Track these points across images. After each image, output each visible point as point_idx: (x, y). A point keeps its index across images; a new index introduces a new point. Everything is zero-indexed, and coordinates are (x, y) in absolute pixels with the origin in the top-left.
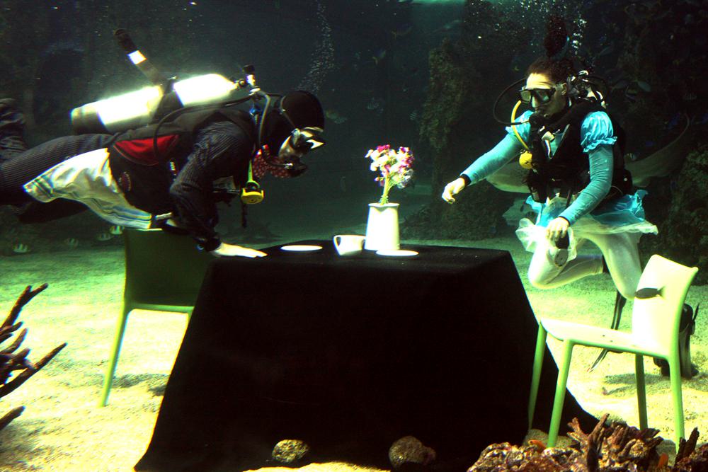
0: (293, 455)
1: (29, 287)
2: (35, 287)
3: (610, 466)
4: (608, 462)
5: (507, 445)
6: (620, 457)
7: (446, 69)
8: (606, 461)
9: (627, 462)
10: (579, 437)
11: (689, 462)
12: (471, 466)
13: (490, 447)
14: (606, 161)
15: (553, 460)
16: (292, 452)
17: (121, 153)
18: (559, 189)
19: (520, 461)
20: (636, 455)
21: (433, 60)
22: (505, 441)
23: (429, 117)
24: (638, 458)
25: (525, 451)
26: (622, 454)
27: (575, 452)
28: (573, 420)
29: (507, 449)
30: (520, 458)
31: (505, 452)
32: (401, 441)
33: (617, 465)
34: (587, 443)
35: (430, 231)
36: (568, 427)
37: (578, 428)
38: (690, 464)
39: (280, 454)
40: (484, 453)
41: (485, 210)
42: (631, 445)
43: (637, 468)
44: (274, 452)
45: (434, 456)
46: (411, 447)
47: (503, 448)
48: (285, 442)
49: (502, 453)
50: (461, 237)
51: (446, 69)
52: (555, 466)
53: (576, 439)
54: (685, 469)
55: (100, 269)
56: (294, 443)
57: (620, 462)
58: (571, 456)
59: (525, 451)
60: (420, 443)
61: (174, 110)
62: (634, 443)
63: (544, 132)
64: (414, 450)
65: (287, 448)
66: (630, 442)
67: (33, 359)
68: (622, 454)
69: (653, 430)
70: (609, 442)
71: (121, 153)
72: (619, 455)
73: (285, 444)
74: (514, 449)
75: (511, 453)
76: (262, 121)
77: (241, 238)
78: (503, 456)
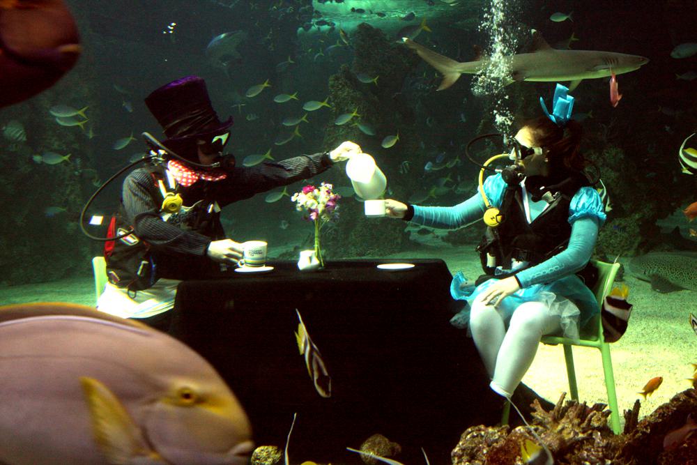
0: (270, 460)
4: (572, 433)
5: (482, 427)
6: (583, 428)
8: (570, 433)
10: (542, 415)
11: (647, 423)
12: (454, 447)
13: (470, 430)
14: (593, 235)
15: (528, 435)
16: (269, 457)
17: (501, 251)
18: (177, 282)
19: (497, 440)
20: (596, 425)
21: (333, 86)
22: (480, 424)
23: (332, 141)
24: (598, 427)
25: (498, 431)
28: (535, 402)
29: (483, 431)
30: (497, 437)
31: (483, 433)
32: (370, 439)
33: (581, 435)
34: (550, 419)
35: (338, 250)
37: (541, 408)
38: (649, 425)
39: (259, 459)
40: (463, 435)
41: (390, 226)
42: (592, 417)
44: (253, 458)
45: (400, 450)
46: (380, 443)
47: (480, 430)
48: (262, 448)
50: (369, 254)
51: (345, 94)
53: (540, 418)
54: (645, 430)
56: (270, 448)
57: (583, 433)
59: (498, 431)
60: (387, 439)
61: (470, 222)
62: (595, 414)
63: (545, 191)
64: (383, 446)
65: (265, 454)
66: (591, 414)
68: (584, 425)
69: (602, 405)
70: (571, 417)
71: (501, 251)
72: (581, 426)
73: (262, 450)
74: (490, 430)
75: (488, 433)
76: (180, 157)
78: (482, 436)
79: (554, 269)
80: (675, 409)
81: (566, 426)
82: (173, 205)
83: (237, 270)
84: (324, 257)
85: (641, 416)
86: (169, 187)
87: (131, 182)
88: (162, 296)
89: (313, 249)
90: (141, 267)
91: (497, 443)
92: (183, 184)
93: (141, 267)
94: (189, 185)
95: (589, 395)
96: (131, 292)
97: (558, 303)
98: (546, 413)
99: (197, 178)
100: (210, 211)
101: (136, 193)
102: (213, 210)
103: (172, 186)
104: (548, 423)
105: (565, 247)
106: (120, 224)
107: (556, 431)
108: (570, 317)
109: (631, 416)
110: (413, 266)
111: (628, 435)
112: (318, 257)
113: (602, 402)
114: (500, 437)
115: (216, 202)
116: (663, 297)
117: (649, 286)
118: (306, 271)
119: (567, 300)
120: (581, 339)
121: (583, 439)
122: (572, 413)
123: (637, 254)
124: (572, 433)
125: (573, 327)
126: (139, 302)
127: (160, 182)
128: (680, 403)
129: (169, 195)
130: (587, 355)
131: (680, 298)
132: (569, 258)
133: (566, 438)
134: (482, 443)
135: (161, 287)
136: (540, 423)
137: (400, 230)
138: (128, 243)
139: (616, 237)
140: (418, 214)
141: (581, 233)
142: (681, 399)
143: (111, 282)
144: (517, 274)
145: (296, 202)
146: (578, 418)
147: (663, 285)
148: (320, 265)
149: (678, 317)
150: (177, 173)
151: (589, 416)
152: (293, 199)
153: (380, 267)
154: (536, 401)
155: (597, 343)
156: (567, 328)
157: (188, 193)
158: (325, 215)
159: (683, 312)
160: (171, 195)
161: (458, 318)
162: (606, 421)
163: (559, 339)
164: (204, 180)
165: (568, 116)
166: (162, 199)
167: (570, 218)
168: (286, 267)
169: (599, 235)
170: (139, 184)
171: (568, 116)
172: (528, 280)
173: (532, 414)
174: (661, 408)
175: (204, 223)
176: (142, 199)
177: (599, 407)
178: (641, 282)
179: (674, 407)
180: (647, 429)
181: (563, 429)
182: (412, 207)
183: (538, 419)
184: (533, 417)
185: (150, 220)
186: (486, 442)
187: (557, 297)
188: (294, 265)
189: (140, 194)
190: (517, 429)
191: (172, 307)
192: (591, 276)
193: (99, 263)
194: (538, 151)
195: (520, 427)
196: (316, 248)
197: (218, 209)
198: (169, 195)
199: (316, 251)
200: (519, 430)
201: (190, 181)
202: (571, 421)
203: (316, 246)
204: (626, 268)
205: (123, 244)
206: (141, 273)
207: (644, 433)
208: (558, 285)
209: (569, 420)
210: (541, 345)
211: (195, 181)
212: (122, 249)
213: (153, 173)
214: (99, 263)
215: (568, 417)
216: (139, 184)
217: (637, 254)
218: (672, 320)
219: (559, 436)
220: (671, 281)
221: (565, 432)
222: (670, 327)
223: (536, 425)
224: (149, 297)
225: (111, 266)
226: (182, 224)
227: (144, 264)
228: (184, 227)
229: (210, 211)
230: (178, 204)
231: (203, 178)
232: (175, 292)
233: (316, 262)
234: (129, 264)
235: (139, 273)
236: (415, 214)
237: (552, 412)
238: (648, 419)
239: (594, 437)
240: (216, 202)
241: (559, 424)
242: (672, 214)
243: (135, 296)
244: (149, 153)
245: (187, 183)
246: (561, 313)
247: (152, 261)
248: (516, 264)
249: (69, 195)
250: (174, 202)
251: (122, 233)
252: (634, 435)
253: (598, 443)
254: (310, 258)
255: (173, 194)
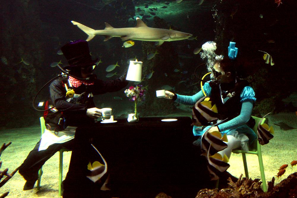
1: (5, 144)
2: (7, 144)
3: (246, 193)
4: (245, 192)
5: (206, 189)
6: (250, 190)
7: (149, 46)
8: (244, 192)
9: (253, 191)
13: (201, 191)
14: (251, 108)
15: (226, 193)
18: (76, 128)
25: (213, 191)
26: (250, 188)
27: (232, 190)
29: (207, 191)
30: (213, 194)
31: (207, 192)
32: (159, 195)
33: (249, 193)
34: (236, 186)
36: (227, 181)
38: (278, 188)
42: (254, 185)
43: (257, 192)
47: (206, 191)
49: (206, 192)
51: (149, 46)
52: (227, 195)
53: (231, 185)
55: (12, 138)
57: (250, 191)
58: (230, 191)
59: (213, 191)
63: (228, 93)
66: (253, 183)
67: (10, 172)
68: (250, 188)
70: (245, 185)
72: (249, 189)
74: (210, 191)
75: (209, 192)
77: (220, 97)
78: (206, 193)
79: (234, 124)
80: (289, 181)
81: (243, 188)
82: (71, 94)
83: (102, 122)
84: (139, 116)
85: (275, 185)
86: (69, 86)
87: (53, 86)
88: (69, 134)
89: (134, 113)
90: (60, 121)
91: (213, 196)
92: (75, 86)
93: (60, 121)
94: (78, 87)
95: (252, 176)
96: (56, 132)
97: (239, 135)
98: (234, 183)
99: (81, 83)
100: (89, 96)
101: (55, 90)
102: (90, 96)
103: (71, 86)
104: (235, 187)
105: (239, 114)
106: (50, 104)
107: (238, 191)
108: (245, 141)
109: (271, 184)
110: (177, 120)
111: (269, 193)
112: (136, 116)
113: (258, 178)
114: (214, 193)
115: (91, 93)
116: (285, 132)
117: (279, 127)
118: (131, 122)
119: (243, 134)
120: (249, 151)
121: (250, 194)
122: (245, 183)
123: (274, 114)
124: (245, 192)
125: (246, 145)
126: (59, 136)
127: (65, 85)
128: (292, 178)
129: (69, 90)
130: (252, 158)
131: (292, 132)
132: (241, 119)
133: (243, 194)
134: (206, 196)
135: (69, 129)
136: (232, 187)
137: (172, 105)
138: (53, 111)
139: (265, 106)
140: (179, 98)
141: (246, 108)
142: (292, 177)
143: (47, 129)
144: (218, 126)
145: (127, 93)
146: (248, 185)
147: (285, 127)
148: (137, 120)
149: (291, 141)
150: (72, 81)
151: (252, 184)
152: (125, 92)
153: (162, 120)
154: (230, 178)
155: (256, 152)
156: (243, 146)
157: (77, 90)
158: (139, 98)
159: (294, 139)
160: (70, 90)
161: (196, 142)
162: (260, 186)
163: (240, 151)
164: (84, 84)
165: (235, 56)
166: (66, 92)
167: (241, 101)
168: (122, 121)
169: (253, 108)
170: (56, 86)
171: (235, 56)
172: (223, 128)
173: (228, 183)
174: (283, 181)
175: (87, 102)
176: (57, 92)
177: (257, 180)
178: (275, 125)
179: (289, 180)
180: (277, 190)
181: (241, 190)
182: (176, 95)
183: (230, 186)
184: (228, 185)
185: (61, 101)
186: (208, 196)
187: (239, 133)
188: (126, 120)
189: (57, 90)
190: (221, 190)
191: (74, 138)
192: (252, 123)
193: (42, 120)
194: (223, 73)
195: (223, 189)
196: (135, 113)
197: (92, 96)
198: (69, 90)
199: (135, 114)
200: (222, 190)
201: (78, 85)
202: (245, 187)
203: (135, 112)
204: (269, 119)
205: (52, 112)
206: (60, 123)
207: (276, 192)
208: (239, 129)
209: (244, 186)
210: (232, 153)
211: (80, 85)
212: (50, 114)
213: (63, 81)
214: (42, 120)
215: (243, 185)
216: (56, 86)
217: (274, 114)
218: (289, 142)
219: (240, 193)
220: (288, 125)
221: (242, 191)
222: (288, 145)
223: (230, 188)
224: (63, 134)
225: (47, 122)
226: (77, 102)
227: (61, 120)
228: (78, 103)
229: (89, 96)
230: (73, 94)
231: (84, 84)
232: (75, 131)
233: (135, 118)
234: (54, 121)
235: (59, 123)
236: (177, 98)
237: (236, 183)
238: (278, 185)
239: (255, 193)
240: (91, 93)
241: (239, 188)
242: (289, 97)
243: (58, 134)
244: (61, 74)
245: (77, 86)
246: (241, 140)
247: (64, 118)
248: (219, 121)
249: (31, 90)
250: (71, 93)
251: (51, 107)
252: (272, 193)
253: (257, 196)
254: (133, 117)
255: (70, 89)
